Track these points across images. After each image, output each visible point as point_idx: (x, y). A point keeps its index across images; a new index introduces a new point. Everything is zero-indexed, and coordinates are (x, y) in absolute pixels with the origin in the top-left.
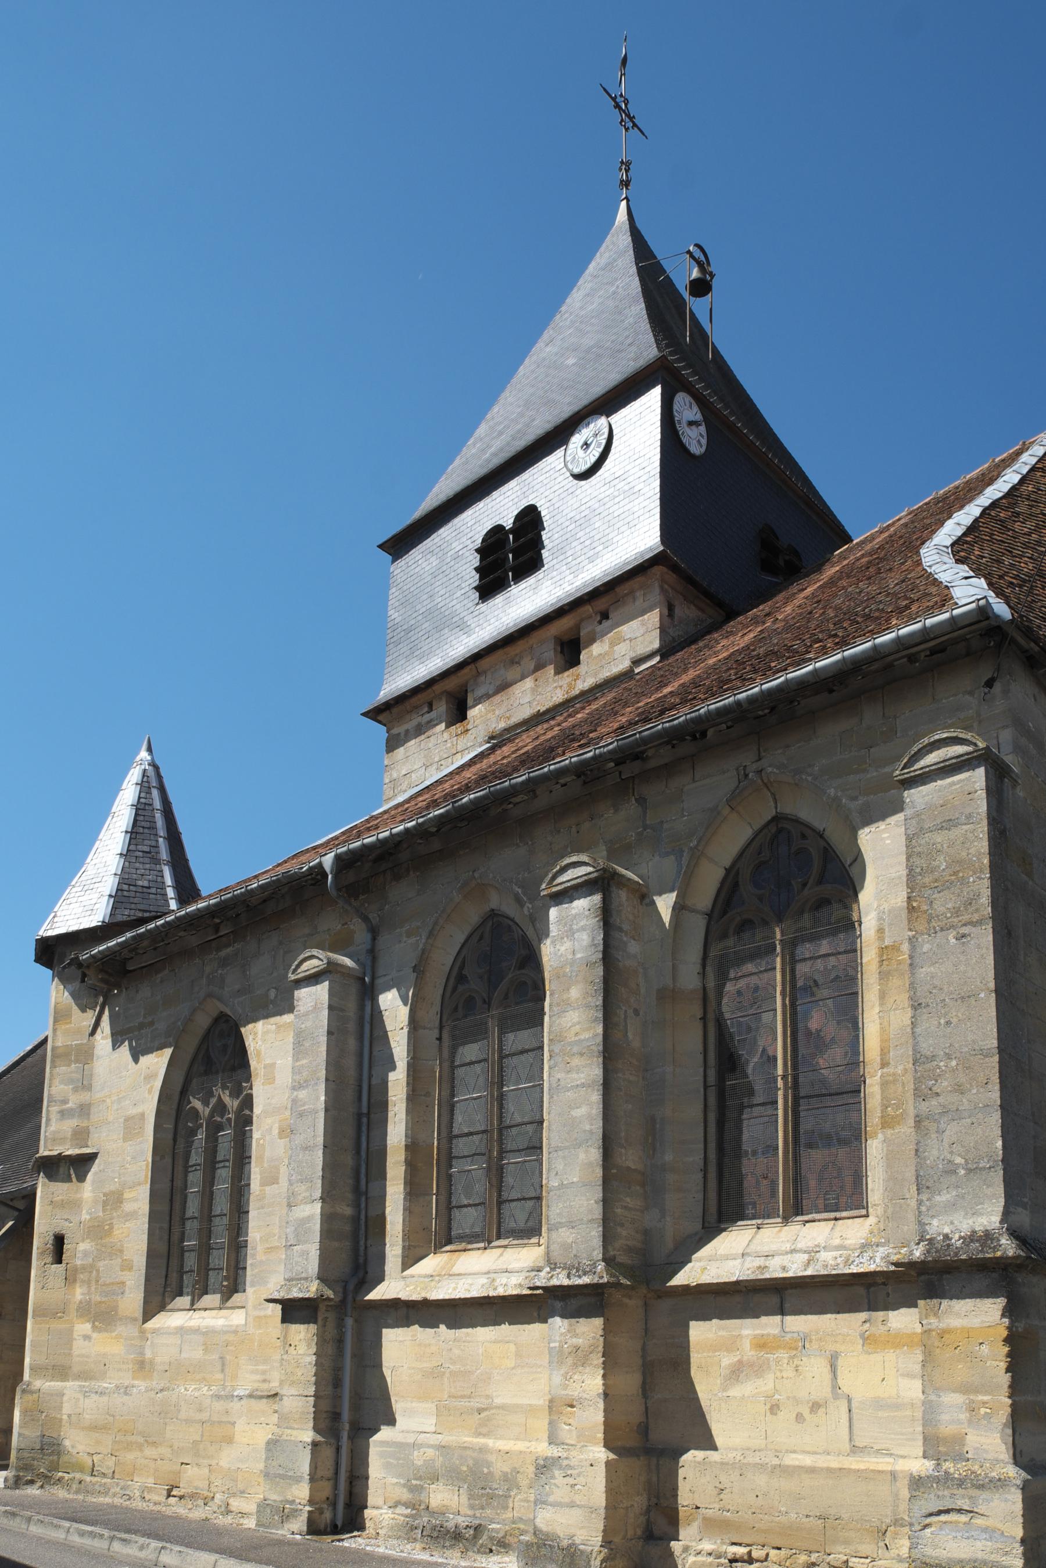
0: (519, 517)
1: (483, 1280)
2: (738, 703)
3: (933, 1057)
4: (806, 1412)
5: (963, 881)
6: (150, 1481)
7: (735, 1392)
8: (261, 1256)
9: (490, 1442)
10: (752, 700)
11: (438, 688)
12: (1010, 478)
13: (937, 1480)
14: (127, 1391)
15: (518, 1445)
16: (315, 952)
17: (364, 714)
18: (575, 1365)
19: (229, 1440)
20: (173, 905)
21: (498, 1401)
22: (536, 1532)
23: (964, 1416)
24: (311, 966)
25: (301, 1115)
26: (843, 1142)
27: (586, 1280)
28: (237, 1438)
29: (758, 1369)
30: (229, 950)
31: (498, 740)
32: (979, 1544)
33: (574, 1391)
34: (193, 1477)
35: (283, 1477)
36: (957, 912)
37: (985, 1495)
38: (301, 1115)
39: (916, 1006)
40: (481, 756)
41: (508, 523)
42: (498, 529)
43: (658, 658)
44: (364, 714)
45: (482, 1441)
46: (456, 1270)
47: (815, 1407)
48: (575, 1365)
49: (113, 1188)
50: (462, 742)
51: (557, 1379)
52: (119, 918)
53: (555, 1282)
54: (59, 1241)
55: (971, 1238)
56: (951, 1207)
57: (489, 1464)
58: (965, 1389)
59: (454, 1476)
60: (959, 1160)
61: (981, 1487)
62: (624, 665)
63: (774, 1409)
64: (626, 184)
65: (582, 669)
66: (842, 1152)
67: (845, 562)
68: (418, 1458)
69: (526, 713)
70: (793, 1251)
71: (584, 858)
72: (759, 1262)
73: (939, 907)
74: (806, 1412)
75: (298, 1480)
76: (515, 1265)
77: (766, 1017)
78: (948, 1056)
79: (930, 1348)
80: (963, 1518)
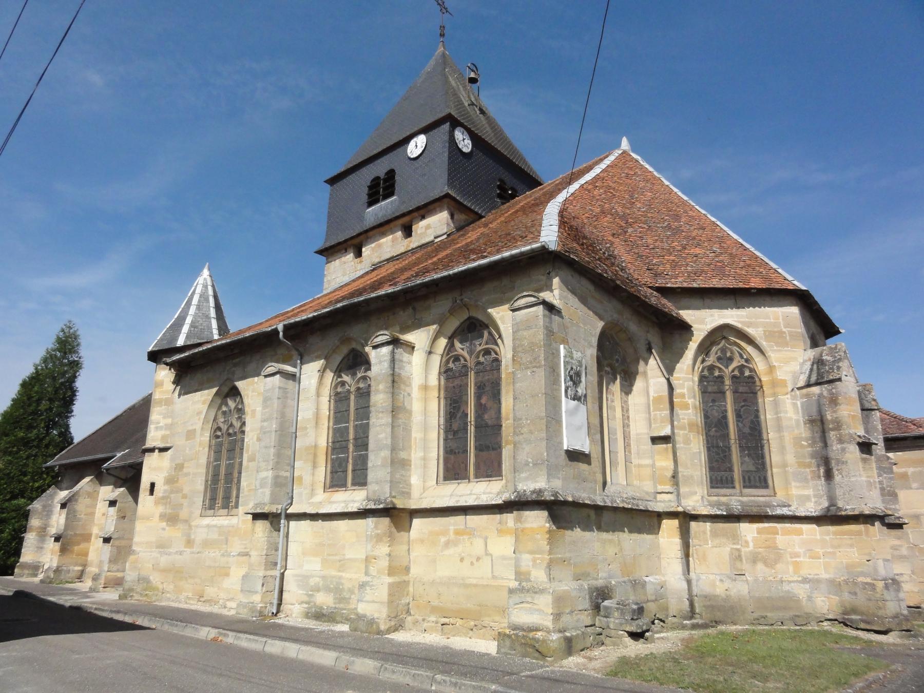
0: (387, 174)
1: (343, 505)
2: (450, 275)
3: (521, 419)
4: (475, 562)
5: (533, 350)
6: (190, 595)
7: (447, 552)
8: (246, 493)
9: (344, 574)
10: (455, 274)
11: (349, 243)
12: (597, 170)
13: (519, 590)
14: (181, 553)
15: (352, 576)
16: (273, 364)
17: (316, 252)
18: (377, 542)
19: (227, 575)
20: (216, 337)
21: (347, 557)
22: (357, 614)
23: (531, 564)
24: (270, 370)
25: (265, 433)
26: (494, 449)
27: (381, 506)
28: (231, 573)
29: (455, 543)
30: (237, 360)
31: (376, 267)
32: (535, 616)
33: (376, 553)
34: (210, 592)
35: (249, 591)
36: (531, 362)
37: (537, 596)
38: (265, 433)
39: (515, 398)
40: (367, 273)
41: (382, 176)
42: (378, 178)
43: (445, 236)
44: (316, 252)
45: (340, 574)
46: (332, 500)
47: (478, 559)
48: (377, 542)
49: (180, 462)
50: (359, 266)
51: (369, 547)
52: (189, 343)
53: (369, 507)
54: (153, 485)
55: (533, 492)
56: (527, 479)
57: (342, 584)
58: (531, 552)
59: (328, 590)
60: (530, 460)
61: (536, 593)
62: (432, 238)
63: (462, 560)
64: (442, 35)
65: (413, 238)
66: (493, 453)
67: (435, 259)
68: (312, 582)
69: (388, 256)
70: (471, 494)
71: (386, 332)
72: (457, 498)
73: (524, 360)
74: (475, 562)
75: (256, 592)
76: (357, 498)
77: (464, 398)
78: (527, 419)
79: (518, 535)
80: (529, 606)
